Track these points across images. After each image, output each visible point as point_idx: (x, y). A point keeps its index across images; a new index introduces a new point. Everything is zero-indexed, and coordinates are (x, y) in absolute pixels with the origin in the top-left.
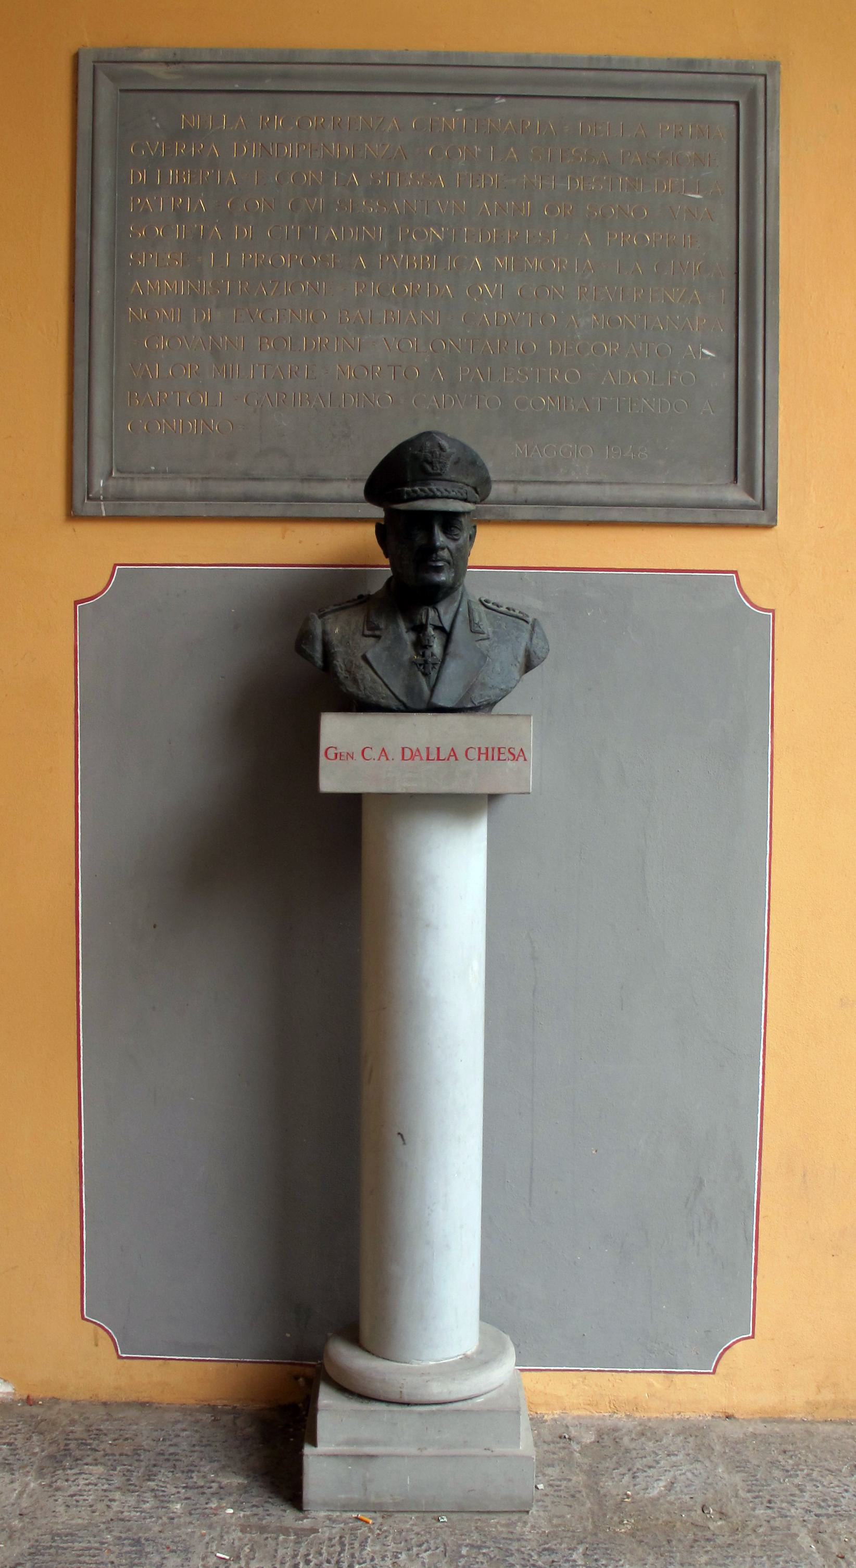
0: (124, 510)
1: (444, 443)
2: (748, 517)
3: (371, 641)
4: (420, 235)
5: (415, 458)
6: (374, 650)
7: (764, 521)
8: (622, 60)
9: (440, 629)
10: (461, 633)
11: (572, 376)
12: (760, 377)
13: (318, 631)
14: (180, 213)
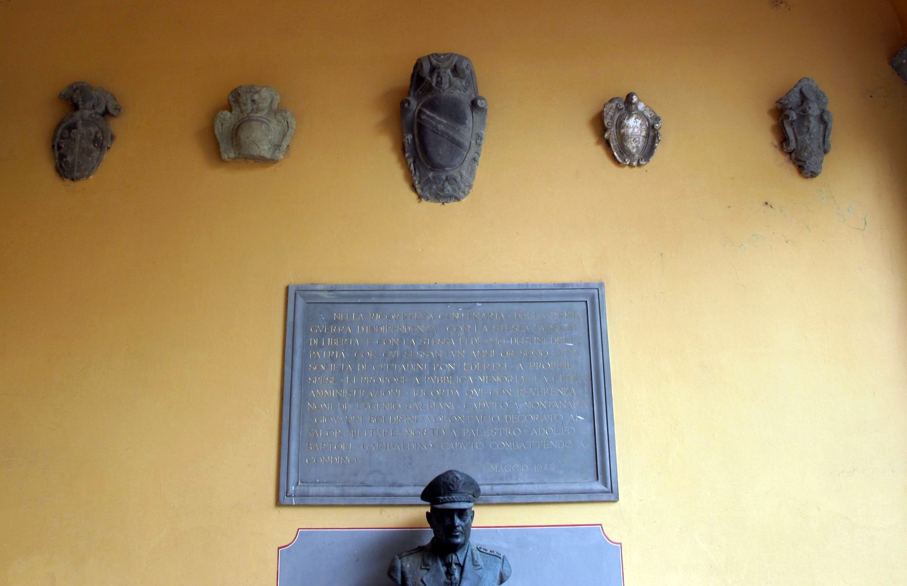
0: (304, 501)
1: (458, 475)
2: (605, 497)
3: (425, 571)
4: (444, 367)
5: (445, 483)
6: (427, 577)
7: (613, 499)
8: (533, 285)
9: (458, 564)
10: (468, 566)
11: (517, 432)
12: (606, 429)
13: (399, 566)
14: (333, 359)
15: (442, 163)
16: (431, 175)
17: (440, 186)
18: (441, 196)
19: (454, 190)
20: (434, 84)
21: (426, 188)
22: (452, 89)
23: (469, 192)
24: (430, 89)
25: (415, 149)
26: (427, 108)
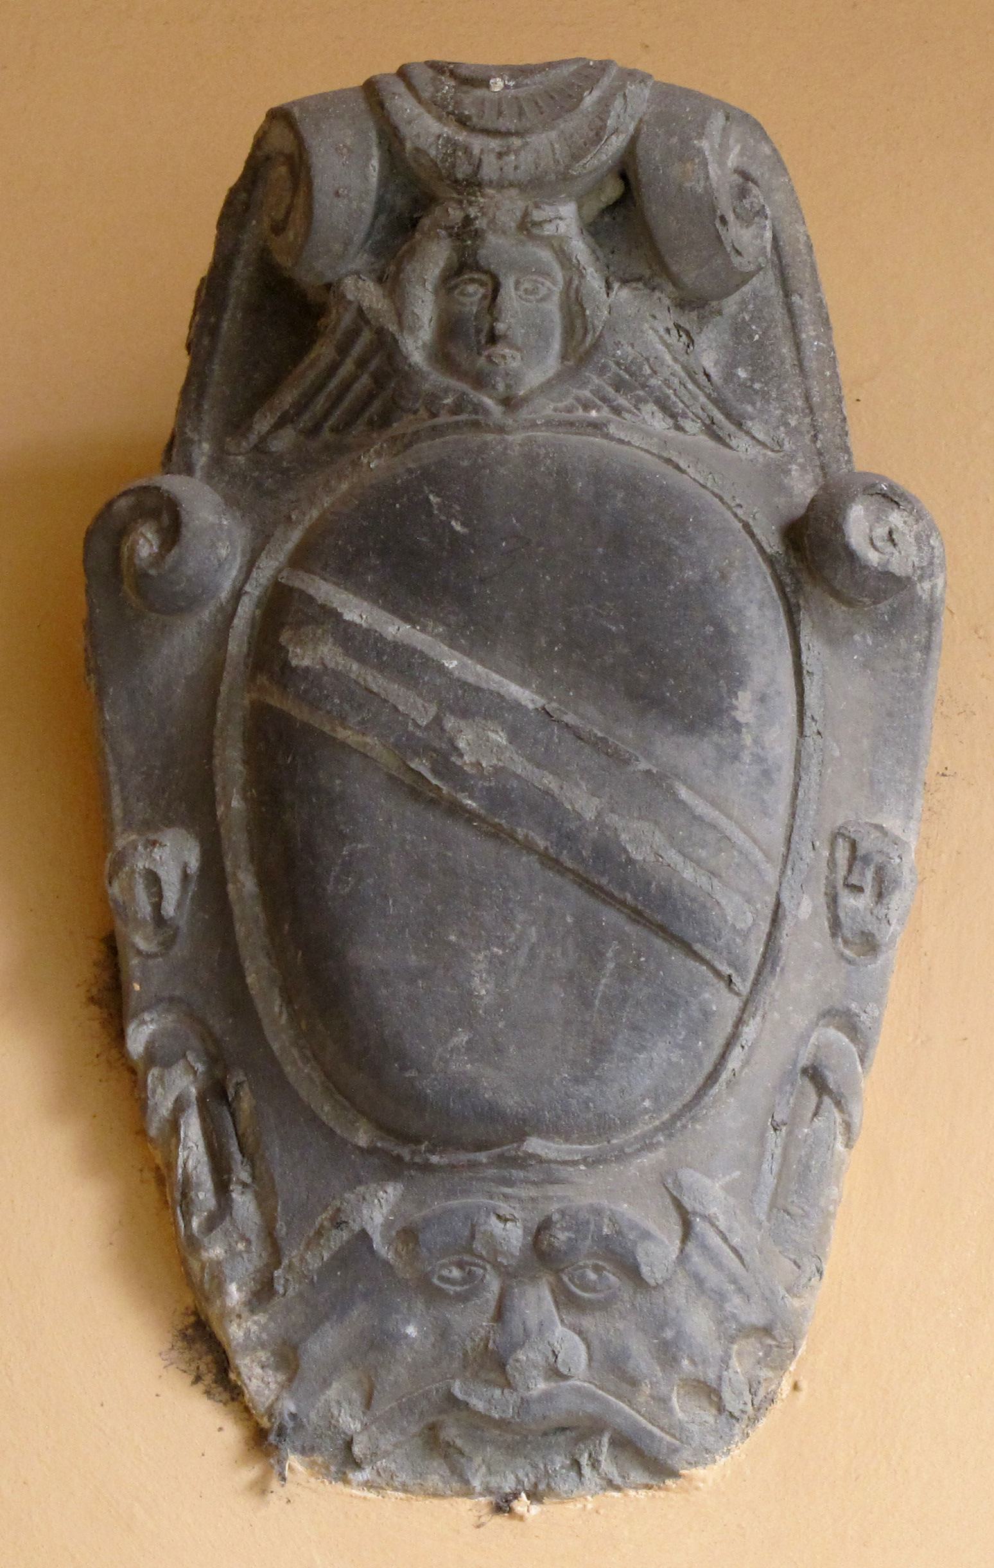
15: (500, 1086)
16: (378, 1209)
17: (472, 1321)
18: (480, 1425)
19: (615, 1367)
20: (416, 347)
21: (326, 1343)
22: (584, 391)
23: (763, 1404)
24: (383, 393)
25: (231, 967)
26: (347, 573)
